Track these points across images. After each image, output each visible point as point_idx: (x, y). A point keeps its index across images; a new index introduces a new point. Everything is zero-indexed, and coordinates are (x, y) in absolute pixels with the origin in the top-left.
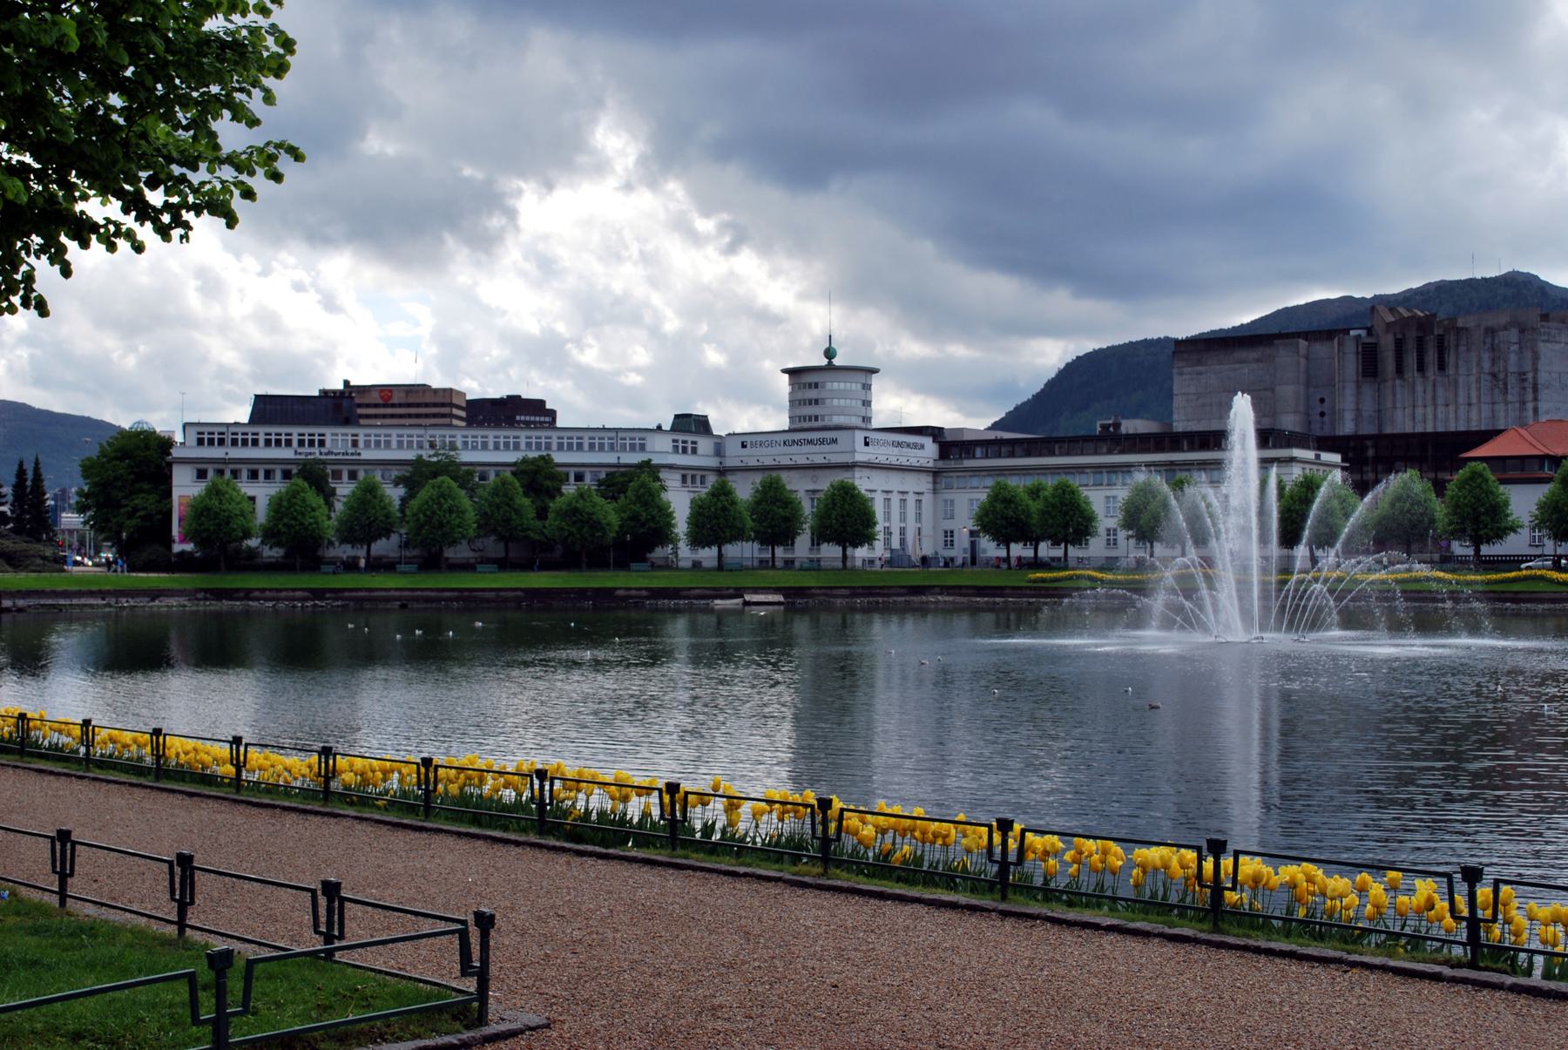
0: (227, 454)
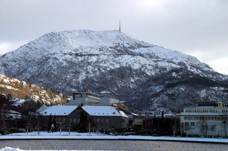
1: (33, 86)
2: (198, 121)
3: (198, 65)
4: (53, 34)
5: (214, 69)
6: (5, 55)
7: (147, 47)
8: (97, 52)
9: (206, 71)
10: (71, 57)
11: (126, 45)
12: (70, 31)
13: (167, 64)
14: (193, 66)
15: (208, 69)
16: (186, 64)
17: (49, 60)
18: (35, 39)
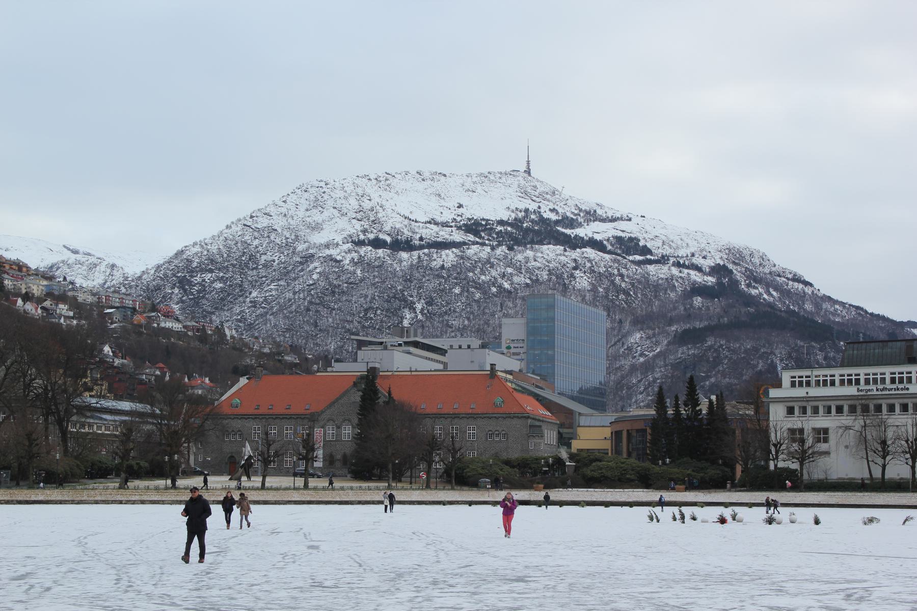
0: (807, 393)
1: (176, 291)
2: (846, 419)
3: (770, 273)
4: (323, 184)
5: (816, 286)
6: (182, 251)
7: (613, 220)
8: (458, 237)
9: (796, 294)
10: (380, 252)
11: (548, 215)
12: (375, 176)
13: (675, 271)
14: (756, 281)
15: (801, 286)
16: (735, 272)
17: (312, 266)
18: (271, 203)
